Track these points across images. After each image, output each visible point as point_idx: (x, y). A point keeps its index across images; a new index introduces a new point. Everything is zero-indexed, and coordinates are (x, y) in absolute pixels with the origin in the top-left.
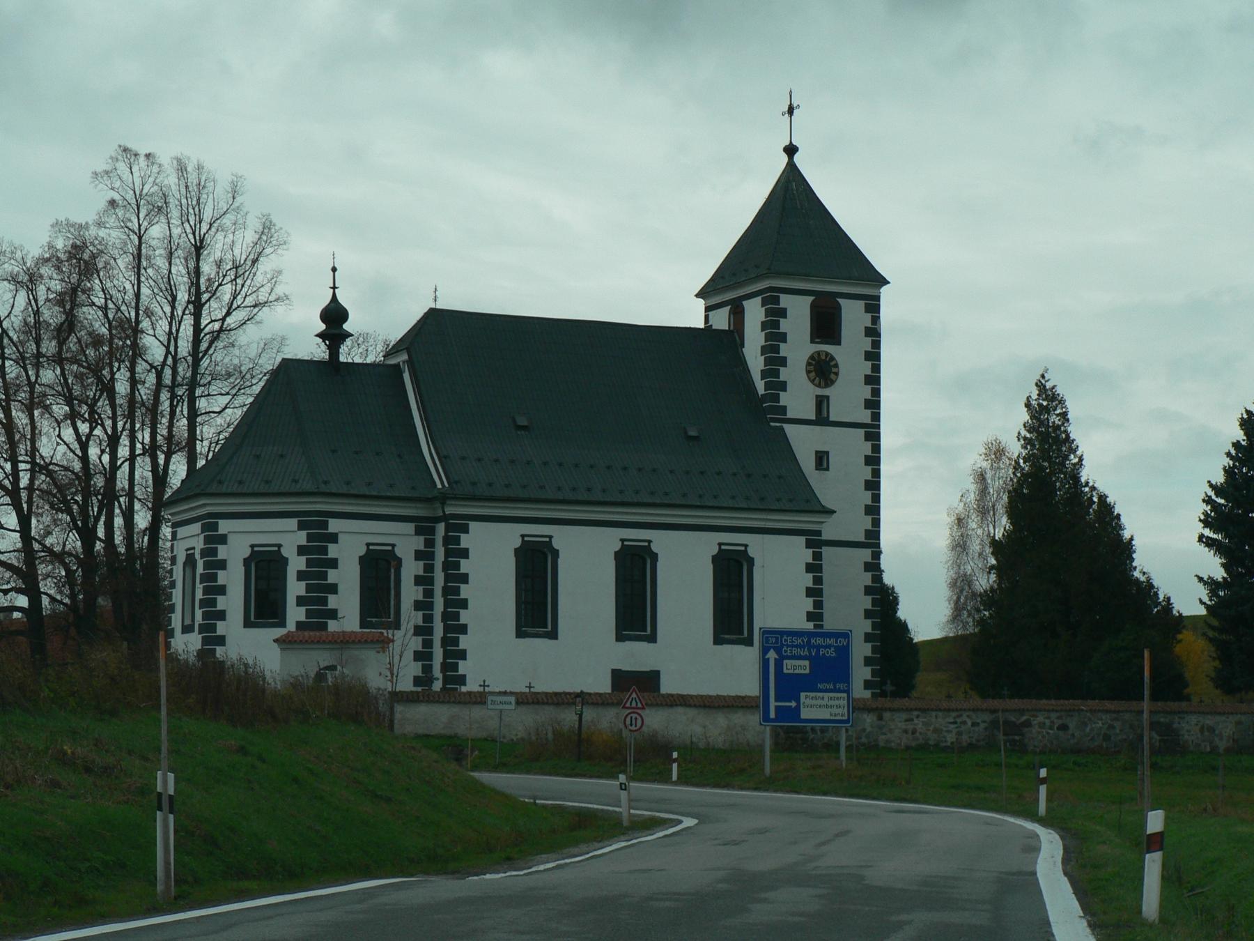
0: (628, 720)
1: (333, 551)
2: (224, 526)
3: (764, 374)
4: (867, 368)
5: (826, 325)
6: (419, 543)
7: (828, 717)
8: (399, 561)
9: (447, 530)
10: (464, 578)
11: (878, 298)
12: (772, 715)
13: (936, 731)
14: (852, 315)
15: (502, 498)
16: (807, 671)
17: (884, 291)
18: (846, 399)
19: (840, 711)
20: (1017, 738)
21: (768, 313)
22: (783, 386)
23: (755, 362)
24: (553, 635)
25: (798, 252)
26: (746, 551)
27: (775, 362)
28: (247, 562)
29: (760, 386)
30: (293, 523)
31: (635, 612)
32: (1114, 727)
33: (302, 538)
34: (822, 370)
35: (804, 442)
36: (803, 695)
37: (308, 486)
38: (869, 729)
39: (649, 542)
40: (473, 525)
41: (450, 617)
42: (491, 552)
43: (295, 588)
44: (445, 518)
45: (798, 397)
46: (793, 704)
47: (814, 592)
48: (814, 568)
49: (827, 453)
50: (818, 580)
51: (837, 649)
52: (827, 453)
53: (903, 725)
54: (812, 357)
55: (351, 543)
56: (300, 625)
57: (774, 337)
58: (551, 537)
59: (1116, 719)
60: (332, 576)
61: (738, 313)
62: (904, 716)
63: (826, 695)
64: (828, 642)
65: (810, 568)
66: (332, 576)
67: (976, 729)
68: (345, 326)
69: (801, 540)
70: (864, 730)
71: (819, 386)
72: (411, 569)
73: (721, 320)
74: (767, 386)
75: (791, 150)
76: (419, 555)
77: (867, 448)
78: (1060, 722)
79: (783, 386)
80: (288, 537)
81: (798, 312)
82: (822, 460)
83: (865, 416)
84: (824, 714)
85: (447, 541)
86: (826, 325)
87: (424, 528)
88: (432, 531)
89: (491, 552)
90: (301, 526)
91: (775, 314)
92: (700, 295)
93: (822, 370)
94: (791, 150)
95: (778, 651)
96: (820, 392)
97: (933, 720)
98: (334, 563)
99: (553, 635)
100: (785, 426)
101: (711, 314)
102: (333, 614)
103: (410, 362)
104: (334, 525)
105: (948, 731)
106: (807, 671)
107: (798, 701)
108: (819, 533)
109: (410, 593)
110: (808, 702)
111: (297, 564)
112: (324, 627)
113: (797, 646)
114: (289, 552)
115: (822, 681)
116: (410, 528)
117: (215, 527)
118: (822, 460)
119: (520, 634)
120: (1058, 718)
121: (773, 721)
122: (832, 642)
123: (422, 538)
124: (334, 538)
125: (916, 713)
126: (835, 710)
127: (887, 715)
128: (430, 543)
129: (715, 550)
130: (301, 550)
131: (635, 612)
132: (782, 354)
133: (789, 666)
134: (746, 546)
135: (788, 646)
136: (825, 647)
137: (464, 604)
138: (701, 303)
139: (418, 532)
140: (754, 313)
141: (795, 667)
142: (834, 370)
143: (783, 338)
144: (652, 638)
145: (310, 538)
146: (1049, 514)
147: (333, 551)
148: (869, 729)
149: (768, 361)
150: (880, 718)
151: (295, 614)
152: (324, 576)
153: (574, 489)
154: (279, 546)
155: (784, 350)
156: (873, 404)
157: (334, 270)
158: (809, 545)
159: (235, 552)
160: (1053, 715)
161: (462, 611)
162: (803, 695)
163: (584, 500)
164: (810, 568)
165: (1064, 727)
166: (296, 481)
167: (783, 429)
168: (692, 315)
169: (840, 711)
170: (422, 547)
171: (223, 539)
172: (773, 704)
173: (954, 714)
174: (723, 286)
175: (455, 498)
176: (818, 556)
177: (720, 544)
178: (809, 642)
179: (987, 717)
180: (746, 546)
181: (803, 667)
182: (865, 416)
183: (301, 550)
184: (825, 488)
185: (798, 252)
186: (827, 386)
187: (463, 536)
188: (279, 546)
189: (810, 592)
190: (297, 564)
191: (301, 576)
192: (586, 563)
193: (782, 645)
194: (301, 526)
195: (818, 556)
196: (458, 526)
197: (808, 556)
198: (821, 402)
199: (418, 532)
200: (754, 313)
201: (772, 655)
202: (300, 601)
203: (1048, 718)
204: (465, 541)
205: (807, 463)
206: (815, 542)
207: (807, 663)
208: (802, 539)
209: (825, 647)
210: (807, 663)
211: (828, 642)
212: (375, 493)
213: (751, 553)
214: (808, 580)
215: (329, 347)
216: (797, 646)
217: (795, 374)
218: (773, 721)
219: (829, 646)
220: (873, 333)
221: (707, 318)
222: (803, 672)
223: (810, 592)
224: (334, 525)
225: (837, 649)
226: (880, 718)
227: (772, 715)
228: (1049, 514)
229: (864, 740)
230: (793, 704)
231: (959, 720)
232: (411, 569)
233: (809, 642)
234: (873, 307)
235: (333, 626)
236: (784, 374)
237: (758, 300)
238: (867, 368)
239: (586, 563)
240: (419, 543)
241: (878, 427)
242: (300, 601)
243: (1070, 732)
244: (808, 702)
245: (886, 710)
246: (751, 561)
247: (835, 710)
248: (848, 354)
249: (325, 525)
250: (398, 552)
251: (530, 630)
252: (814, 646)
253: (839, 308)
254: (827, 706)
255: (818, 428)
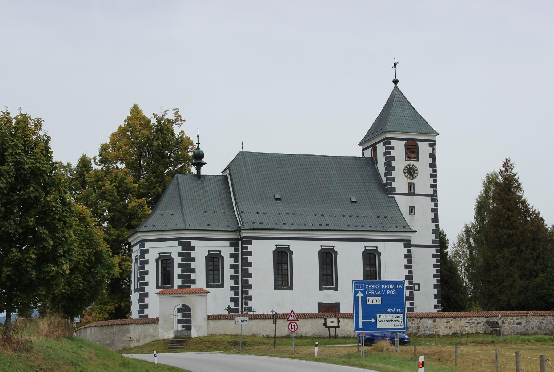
0: (296, 328)
1: (193, 254)
2: (147, 245)
3: (386, 174)
4: (431, 170)
5: (412, 150)
6: (232, 250)
7: (393, 327)
8: (223, 258)
9: (242, 244)
10: (250, 265)
11: (434, 141)
12: (361, 327)
13: (460, 326)
14: (423, 148)
15: (267, 230)
16: (380, 303)
17: (437, 138)
18: (422, 183)
19: (399, 323)
20: (498, 329)
21: (386, 148)
22: (394, 179)
23: (382, 169)
24: (291, 288)
25: (400, 126)
26: (377, 249)
27: (389, 168)
28: (157, 261)
29: (384, 179)
30: (176, 243)
31: (328, 276)
32: (542, 323)
33: (179, 249)
34: (411, 172)
35: (403, 203)
36: (378, 315)
37: (182, 227)
38: (429, 327)
39: (334, 246)
40: (253, 241)
41: (245, 281)
42: (262, 253)
43: (177, 271)
44: (241, 239)
45: (401, 183)
46: (373, 320)
47: (409, 267)
48: (408, 256)
49: (414, 207)
50: (410, 262)
51: (397, 290)
52: (414, 207)
53: (445, 324)
54: (406, 167)
55: (201, 251)
56: (179, 287)
57: (389, 158)
58: (289, 246)
59: (543, 319)
60: (193, 265)
61: (375, 150)
62: (445, 320)
63: (391, 315)
64: (392, 286)
65: (406, 256)
66: (193, 265)
67: (479, 325)
68: (203, 160)
69: (402, 244)
70: (427, 327)
71: (410, 179)
72: (228, 261)
73: (369, 153)
74: (387, 180)
75: (396, 82)
76: (231, 255)
77: (432, 205)
78: (518, 321)
79: (394, 179)
80: (174, 249)
81: (399, 148)
82: (412, 210)
83: (431, 191)
84: (391, 325)
85: (243, 248)
86: (412, 150)
87: (233, 243)
88: (237, 245)
89: (262, 253)
90: (179, 244)
91: (389, 149)
92: (360, 144)
93: (411, 172)
94: (396, 82)
95: (363, 292)
96: (410, 181)
97: (459, 321)
98: (193, 260)
99: (291, 288)
100: (395, 196)
101: (365, 152)
102: (194, 282)
103: (230, 174)
104: (193, 243)
105: (466, 327)
106: (380, 303)
107: (375, 318)
108: (410, 241)
109: (228, 272)
110: (381, 319)
111: (178, 260)
112: (190, 287)
113: (374, 290)
114: (174, 255)
115: (388, 308)
116: (227, 243)
117: (143, 246)
118: (412, 210)
119: (276, 288)
120: (517, 319)
121: (361, 330)
122: (394, 286)
123: (233, 248)
124: (193, 249)
125: (451, 319)
126: (396, 323)
127: (437, 320)
128: (236, 250)
129: (363, 250)
130: (180, 255)
131: (328, 276)
132: (393, 166)
133: (370, 300)
134: (377, 247)
135: (369, 289)
136: (390, 289)
137: (250, 276)
138: (361, 148)
139: (231, 245)
140: (381, 148)
141: (373, 301)
142: (416, 172)
143: (393, 158)
144: (336, 289)
145: (183, 249)
146: (502, 198)
147: (193, 254)
148: (429, 327)
149: (387, 169)
150: (434, 321)
151: (177, 282)
152: (189, 265)
153: (299, 225)
154: (170, 253)
155: (394, 164)
156: (434, 186)
157: (198, 136)
158: (405, 246)
159: (152, 257)
160: (514, 318)
161: (249, 279)
162: (378, 315)
163: (304, 231)
164: (406, 256)
165: (520, 324)
166: (177, 225)
167: (394, 197)
168: (358, 152)
169: (399, 323)
170: (233, 252)
171: (147, 251)
172: (361, 320)
173: (469, 319)
174: (369, 141)
175: (245, 229)
176: (409, 251)
177: (365, 247)
178: (381, 287)
179: (484, 320)
180: (377, 247)
181: (378, 300)
182: (431, 191)
183: (180, 255)
184: (413, 222)
185: (400, 126)
186: (413, 178)
187: (249, 246)
188: (170, 253)
189: (406, 267)
190: (178, 260)
191: (179, 266)
192: (305, 257)
193: (366, 289)
194: (179, 244)
195: (409, 251)
196: (247, 241)
197: (405, 251)
198: (411, 186)
199: (231, 245)
200: (381, 148)
201: (360, 294)
202: (179, 277)
203: (512, 319)
204: (250, 248)
205: (405, 211)
206: (408, 245)
207: (380, 298)
208: (402, 244)
209: (390, 289)
210: (380, 298)
211: (392, 286)
212: (211, 229)
213: (379, 250)
214: (406, 261)
215: (197, 169)
216: (374, 290)
217: (399, 174)
218: (361, 330)
219: (393, 289)
220: (433, 156)
221: (363, 153)
222: (378, 303)
223: (406, 267)
224: (193, 243)
225: (397, 290)
226: (434, 321)
227: (361, 327)
228: (502, 198)
229: (427, 332)
230: (373, 320)
231: (471, 321)
232: (228, 261)
233: (381, 287)
234: (432, 144)
235: (193, 286)
236: (394, 174)
237: (382, 143)
238: (431, 170)
239: (305, 257)
240: (232, 250)
241: (436, 196)
242: (179, 277)
243: (523, 325)
244: (381, 319)
245: (437, 317)
246: (379, 254)
247: (396, 323)
248: (422, 165)
249: (189, 243)
250: (222, 254)
251: (280, 286)
252: (384, 289)
253: (417, 146)
254: (392, 321)
255: (410, 196)
